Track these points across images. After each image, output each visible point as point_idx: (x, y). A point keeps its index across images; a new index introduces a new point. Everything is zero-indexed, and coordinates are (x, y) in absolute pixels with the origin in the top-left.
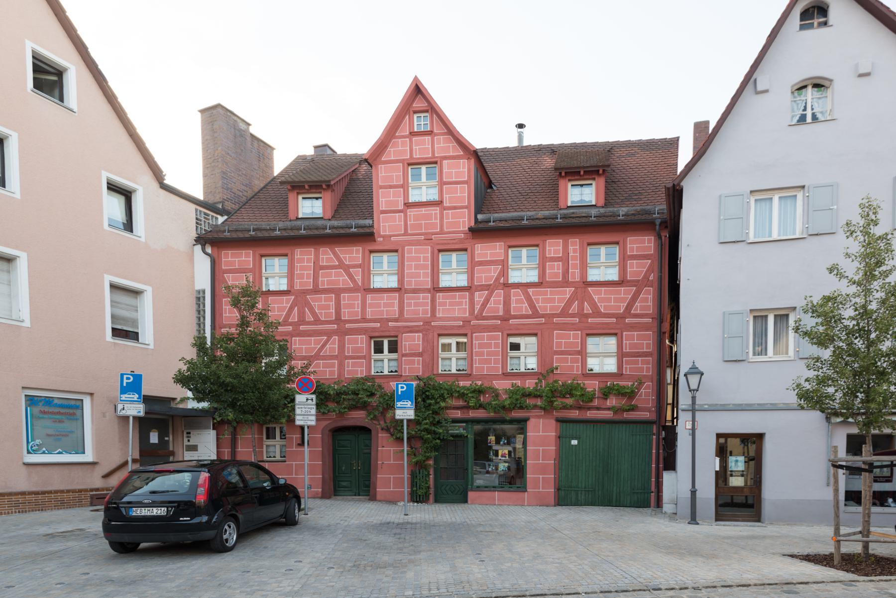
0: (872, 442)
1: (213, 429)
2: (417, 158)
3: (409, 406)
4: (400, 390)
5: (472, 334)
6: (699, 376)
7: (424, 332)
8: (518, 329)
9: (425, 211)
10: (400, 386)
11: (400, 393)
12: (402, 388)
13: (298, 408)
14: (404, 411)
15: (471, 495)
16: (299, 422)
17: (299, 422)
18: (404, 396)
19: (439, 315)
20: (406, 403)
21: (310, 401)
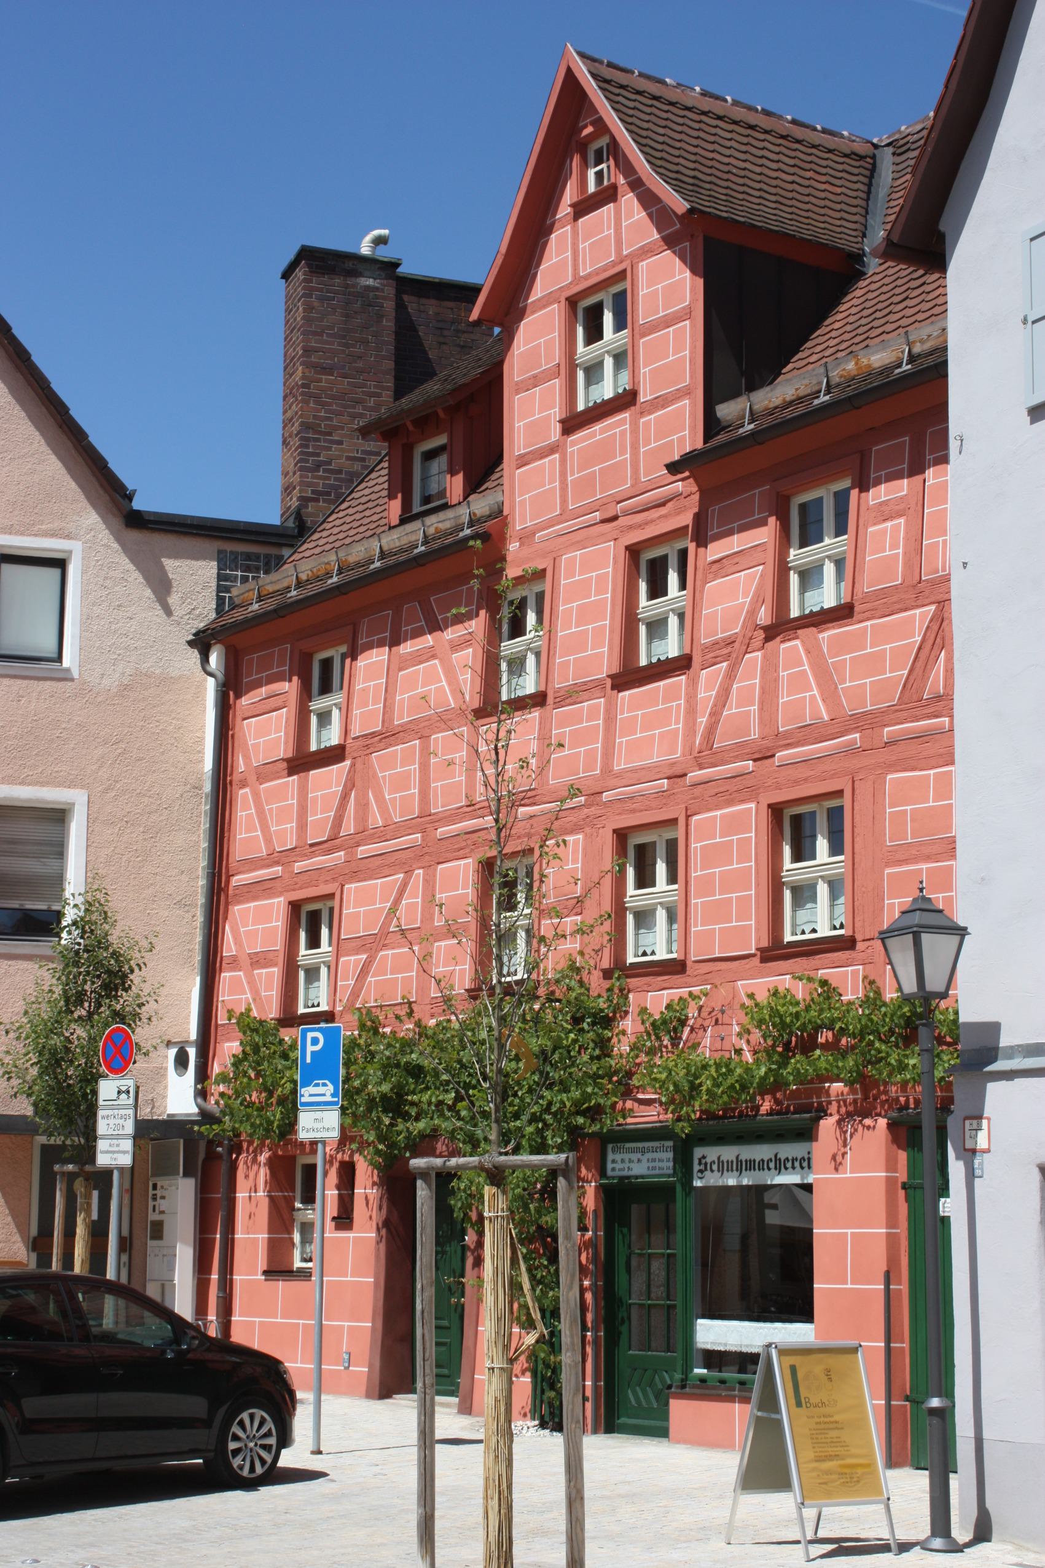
0: (799, 1229)
1: (186, 1174)
2: (589, 275)
3: (328, 1098)
4: (310, 1048)
5: (688, 817)
6: (957, 938)
7: (588, 830)
8: (796, 782)
9: (602, 431)
10: (310, 1035)
11: (308, 1060)
12: (315, 1041)
13: (103, 1117)
14: (318, 1115)
15: (679, 1409)
16: (103, 1160)
17: (103, 1160)
18: (317, 1071)
19: (620, 765)
20: (320, 1090)
21: (124, 1096)
